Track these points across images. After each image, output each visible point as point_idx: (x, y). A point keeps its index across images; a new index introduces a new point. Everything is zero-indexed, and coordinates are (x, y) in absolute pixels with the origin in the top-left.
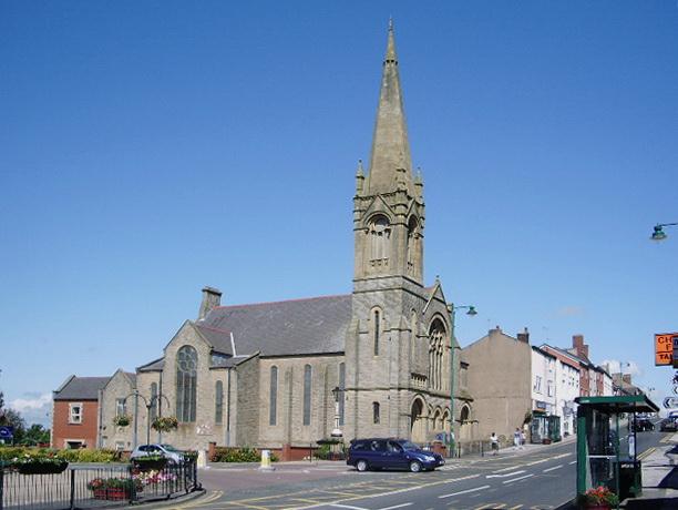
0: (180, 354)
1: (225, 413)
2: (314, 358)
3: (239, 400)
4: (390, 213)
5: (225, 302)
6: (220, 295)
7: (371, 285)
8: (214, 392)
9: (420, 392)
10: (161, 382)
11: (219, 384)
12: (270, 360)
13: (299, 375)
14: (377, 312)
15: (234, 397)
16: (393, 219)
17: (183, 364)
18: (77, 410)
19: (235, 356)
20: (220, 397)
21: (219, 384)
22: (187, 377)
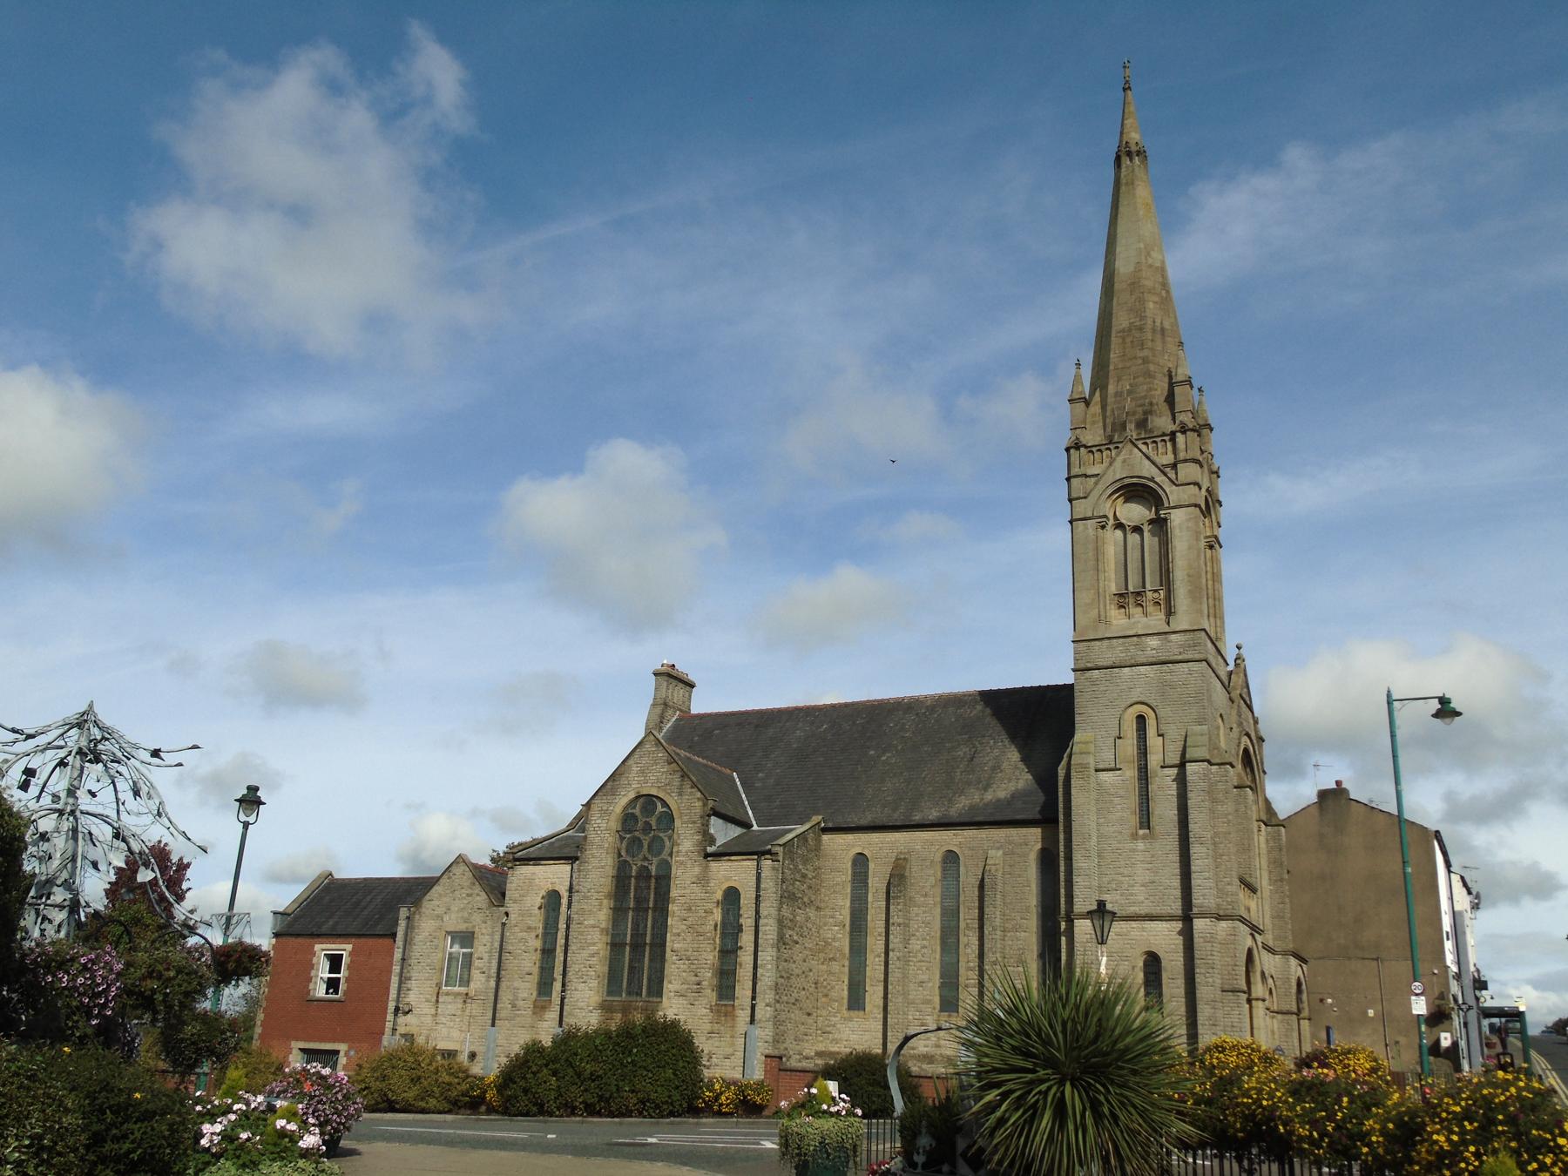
0: (628, 820)
3: (781, 939)
4: (1160, 478)
5: (702, 703)
6: (692, 686)
8: (718, 915)
10: (571, 890)
11: (732, 896)
12: (850, 837)
13: (926, 881)
14: (1141, 719)
15: (769, 929)
16: (1174, 494)
17: (635, 844)
18: (335, 962)
19: (755, 827)
20: (730, 930)
21: (732, 896)
22: (644, 874)
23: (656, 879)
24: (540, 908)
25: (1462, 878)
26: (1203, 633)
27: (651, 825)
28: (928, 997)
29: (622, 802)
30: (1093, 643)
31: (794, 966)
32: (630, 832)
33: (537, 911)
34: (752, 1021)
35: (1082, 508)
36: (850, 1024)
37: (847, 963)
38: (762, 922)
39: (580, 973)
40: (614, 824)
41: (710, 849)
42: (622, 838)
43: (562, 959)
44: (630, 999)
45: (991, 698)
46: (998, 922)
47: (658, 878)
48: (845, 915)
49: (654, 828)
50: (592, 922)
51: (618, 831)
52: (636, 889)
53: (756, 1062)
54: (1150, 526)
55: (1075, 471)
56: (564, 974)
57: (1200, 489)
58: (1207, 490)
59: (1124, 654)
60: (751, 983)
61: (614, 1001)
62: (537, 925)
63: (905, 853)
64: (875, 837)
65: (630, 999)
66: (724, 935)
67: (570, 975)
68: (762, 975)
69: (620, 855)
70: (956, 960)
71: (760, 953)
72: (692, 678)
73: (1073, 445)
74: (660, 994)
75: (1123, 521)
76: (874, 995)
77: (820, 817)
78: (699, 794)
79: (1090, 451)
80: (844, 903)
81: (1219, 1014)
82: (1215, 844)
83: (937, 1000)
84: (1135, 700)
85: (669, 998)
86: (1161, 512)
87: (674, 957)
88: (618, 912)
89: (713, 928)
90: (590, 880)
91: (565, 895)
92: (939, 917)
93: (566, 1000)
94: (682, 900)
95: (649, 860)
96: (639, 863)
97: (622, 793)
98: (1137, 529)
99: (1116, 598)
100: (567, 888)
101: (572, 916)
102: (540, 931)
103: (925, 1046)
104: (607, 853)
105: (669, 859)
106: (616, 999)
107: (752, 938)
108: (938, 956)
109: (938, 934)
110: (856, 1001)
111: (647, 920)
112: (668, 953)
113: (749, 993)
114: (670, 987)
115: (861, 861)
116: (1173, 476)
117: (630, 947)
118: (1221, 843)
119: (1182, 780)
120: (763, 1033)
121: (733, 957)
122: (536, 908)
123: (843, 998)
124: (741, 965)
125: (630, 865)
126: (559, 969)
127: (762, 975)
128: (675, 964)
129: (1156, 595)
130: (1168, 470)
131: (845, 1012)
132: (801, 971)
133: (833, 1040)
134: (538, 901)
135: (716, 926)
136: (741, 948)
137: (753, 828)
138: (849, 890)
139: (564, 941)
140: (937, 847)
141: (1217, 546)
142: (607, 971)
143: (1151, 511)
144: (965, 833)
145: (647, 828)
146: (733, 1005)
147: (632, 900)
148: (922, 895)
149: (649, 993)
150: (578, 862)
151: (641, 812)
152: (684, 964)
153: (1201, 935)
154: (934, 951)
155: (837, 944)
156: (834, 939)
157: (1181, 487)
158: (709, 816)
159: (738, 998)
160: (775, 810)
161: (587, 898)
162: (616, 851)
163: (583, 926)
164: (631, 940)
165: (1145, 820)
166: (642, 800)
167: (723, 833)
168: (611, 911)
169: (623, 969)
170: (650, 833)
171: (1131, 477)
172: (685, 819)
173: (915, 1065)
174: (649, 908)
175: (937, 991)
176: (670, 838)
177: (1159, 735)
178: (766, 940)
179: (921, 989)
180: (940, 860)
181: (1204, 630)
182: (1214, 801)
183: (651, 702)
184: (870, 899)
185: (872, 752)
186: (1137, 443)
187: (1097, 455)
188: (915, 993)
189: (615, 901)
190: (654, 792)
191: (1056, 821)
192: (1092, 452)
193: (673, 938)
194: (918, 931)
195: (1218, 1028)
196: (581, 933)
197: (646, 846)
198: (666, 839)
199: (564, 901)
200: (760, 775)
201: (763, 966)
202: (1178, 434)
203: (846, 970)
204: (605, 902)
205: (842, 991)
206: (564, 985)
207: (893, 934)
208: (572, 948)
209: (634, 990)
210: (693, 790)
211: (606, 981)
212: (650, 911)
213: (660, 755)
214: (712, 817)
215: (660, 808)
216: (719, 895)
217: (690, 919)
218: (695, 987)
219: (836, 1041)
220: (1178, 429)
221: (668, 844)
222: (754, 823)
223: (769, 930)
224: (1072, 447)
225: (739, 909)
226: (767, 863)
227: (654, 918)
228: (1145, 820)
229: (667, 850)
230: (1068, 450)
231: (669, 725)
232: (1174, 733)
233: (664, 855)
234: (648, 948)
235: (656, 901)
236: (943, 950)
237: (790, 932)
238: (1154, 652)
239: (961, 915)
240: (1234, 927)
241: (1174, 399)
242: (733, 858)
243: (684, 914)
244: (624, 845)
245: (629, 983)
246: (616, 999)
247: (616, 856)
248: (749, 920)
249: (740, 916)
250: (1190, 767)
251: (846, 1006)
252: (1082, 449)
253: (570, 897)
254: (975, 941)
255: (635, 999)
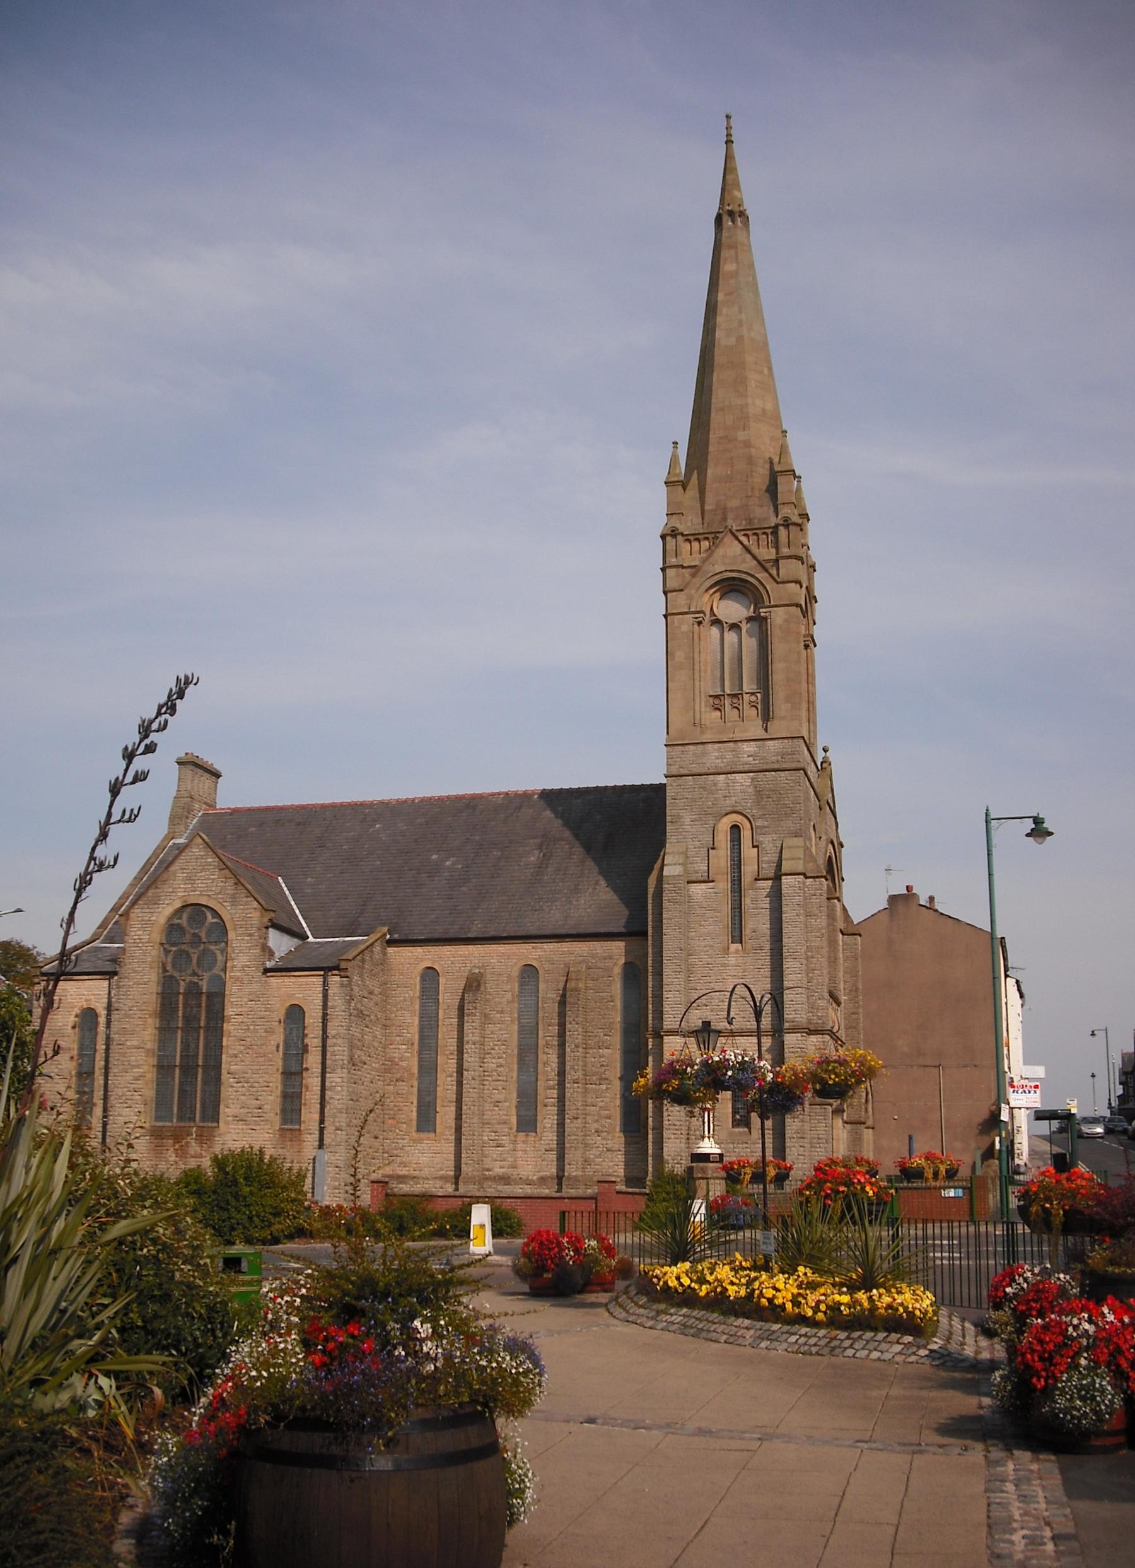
0: (173, 929)
1: (311, 1097)
2: (550, 947)
4: (762, 576)
6: (217, 775)
7: (714, 757)
8: (279, 1037)
9: (358, 1471)
10: (109, 1008)
11: (295, 1014)
12: (418, 951)
14: (735, 828)
17: (181, 958)
19: (311, 939)
20: (294, 1050)
21: (295, 1014)
22: (193, 991)
23: (208, 997)
24: (74, 1027)
25: (1017, 982)
26: (802, 741)
27: (200, 937)
28: (504, 1117)
29: (164, 912)
30: (687, 747)
31: (362, 1087)
32: (174, 944)
33: (70, 1031)
34: (321, 1146)
35: (680, 601)
36: (419, 1146)
37: (416, 1084)
38: (329, 1042)
39: (124, 1098)
40: (157, 936)
41: (269, 965)
42: (167, 952)
43: (102, 1082)
44: (182, 1124)
45: (551, 798)
46: (579, 1040)
47: (210, 996)
48: (413, 1033)
49: (204, 940)
50: (135, 1043)
51: (162, 944)
52: (185, 1008)
53: (326, 1188)
54: (749, 625)
55: (673, 561)
56: (106, 1098)
57: (801, 587)
58: (807, 587)
59: (720, 761)
60: (318, 1106)
61: (164, 1127)
62: (72, 1046)
63: (478, 967)
64: (447, 950)
65: (182, 1124)
66: (286, 1057)
67: (113, 1100)
68: (331, 1098)
69: (165, 970)
70: (534, 1079)
71: (328, 1075)
72: (218, 766)
73: (669, 532)
74: (216, 1118)
75: (720, 617)
76: (445, 1115)
77: (386, 929)
78: (255, 904)
79: (686, 540)
80: (411, 1022)
81: (807, 1126)
82: (807, 958)
83: (514, 1120)
84: (729, 809)
85: (227, 1123)
86: (761, 610)
87: (231, 1080)
88: (165, 1031)
89: (275, 1049)
90: (131, 997)
91: (103, 1013)
92: (516, 1035)
93: (108, 1127)
94: (240, 1019)
95: (198, 976)
96: (188, 979)
97: (167, 902)
98: (735, 627)
99: (711, 699)
100: (105, 1005)
101: (112, 1036)
102: (75, 1052)
103: (501, 1167)
104: (151, 968)
105: (222, 974)
106: (167, 1124)
107: (319, 1059)
108: (515, 1075)
109: (516, 1052)
110: (426, 1120)
111: (198, 1039)
112: (224, 1076)
113: (317, 1116)
114: (227, 1111)
115: (430, 975)
116: (774, 572)
117: (180, 1069)
118: (813, 957)
119: (776, 895)
120: (332, 1158)
121: (298, 1078)
122: (69, 1028)
123: (411, 1120)
124: (307, 1088)
125: (177, 980)
126: (98, 1094)
127: (331, 1098)
128: (232, 1087)
129: (753, 698)
130: (768, 565)
131: (414, 1134)
132: (368, 1093)
133: (401, 1163)
134: (72, 1019)
135: (278, 1047)
136: (307, 1069)
137: (309, 940)
138: (417, 1007)
139: (103, 1063)
140: (514, 961)
141: (812, 645)
142: (154, 1096)
143: (748, 610)
144: (545, 946)
145: (196, 940)
146: (300, 1130)
147: (180, 1019)
148: (498, 1012)
149: (203, 1119)
150: (116, 978)
151: (188, 921)
152: (243, 1087)
153: (791, 1050)
154: (511, 1070)
155: (404, 1064)
156: (401, 1059)
157: (781, 585)
158: (267, 928)
159: (304, 1122)
160: (332, 920)
161: (129, 1016)
162: (161, 965)
163: (125, 1047)
164: (181, 1062)
165: (737, 936)
166: (189, 910)
167: (281, 944)
168: (157, 1032)
169: (173, 1092)
170: (199, 946)
171: (731, 571)
172: (240, 931)
173: (490, 1187)
174: (200, 1027)
175: (514, 1111)
176: (224, 951)
177: (754, 847)
178: (335, 1060)
179: (497, 1108)
180: (517, 974)
181: (803, 737)
182: (808, 915)
183: (175, 794)
184: (441, 1016)
185: (434, 857)
186: (737, 534)
187: (695, 545)
188: (490, 1113)
189: (161, 1021)
190: (203, 901)
191: (645, 934)
192: (690, 541)
193: (229, 1059)
194: (493, 1049)
195: (805, 1141)
196: (124, 1055)
197: (195, 961)
198: (218, 953)
199: (102, 1020)
200: (309, 879)
201: (332, 1088)
202: (781, 528)
203: (415, 1090)
204: (150, 1021)
205: (412, 1112)
206: (105, 1110)
207: (467, 1053)
208: (114, 1070)
209: (185, 1113)
210: (249, 899)
211: (154, 1106)
212: (202, 1031)
213: (209, 860)
214: (270, 929)
215: (210, 918)
216: (281, 1014)
217: (249, 1039)
218: (256, 1111)
219: (404, 1164)
220: (781, 522)
221: (220, 957)
222: (309, 933)
223: (339, 1051)
224: (668, 535)
225: (304, 1028)
226: (335, 980)
227: (206, 1038)
228: (737, 936)
229: (220, 965)
230: (663, 537)
231: (195, 821)
232: (769, 843)
233: (216, 970)
234: (200, 1070)
235: (208, 1019)
236: (520, 1069)
237: (359, 1052)
238: (751, 759)
239: (540, 1032)
240: (824, 1042)
241: (711, 399)
242: (293, 974)
243: (241, 1034)
244: (169, 959)
245: (180, 1108)
246: (167, 1124)
247: (161, 971)
248: (316, 1040)
249: (305, 1036)
250: (785, 880)
251: (414, 1128)
252: (680, 538)
253: (109, 1015)
254: (554, 1058)
255: (187, 1124)
